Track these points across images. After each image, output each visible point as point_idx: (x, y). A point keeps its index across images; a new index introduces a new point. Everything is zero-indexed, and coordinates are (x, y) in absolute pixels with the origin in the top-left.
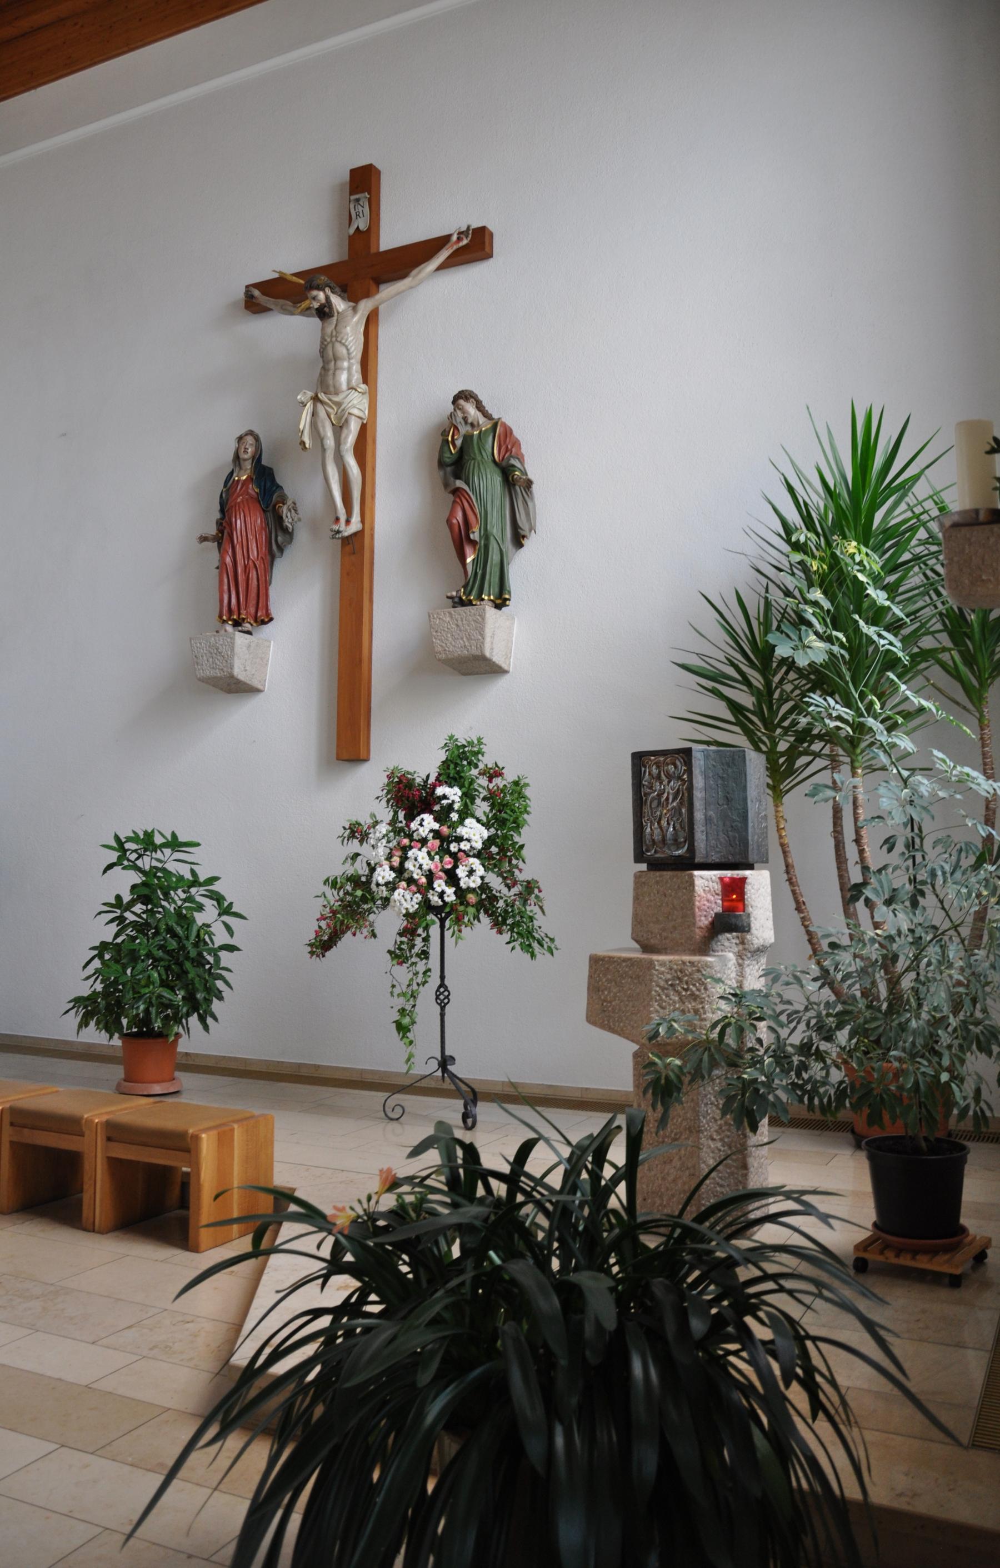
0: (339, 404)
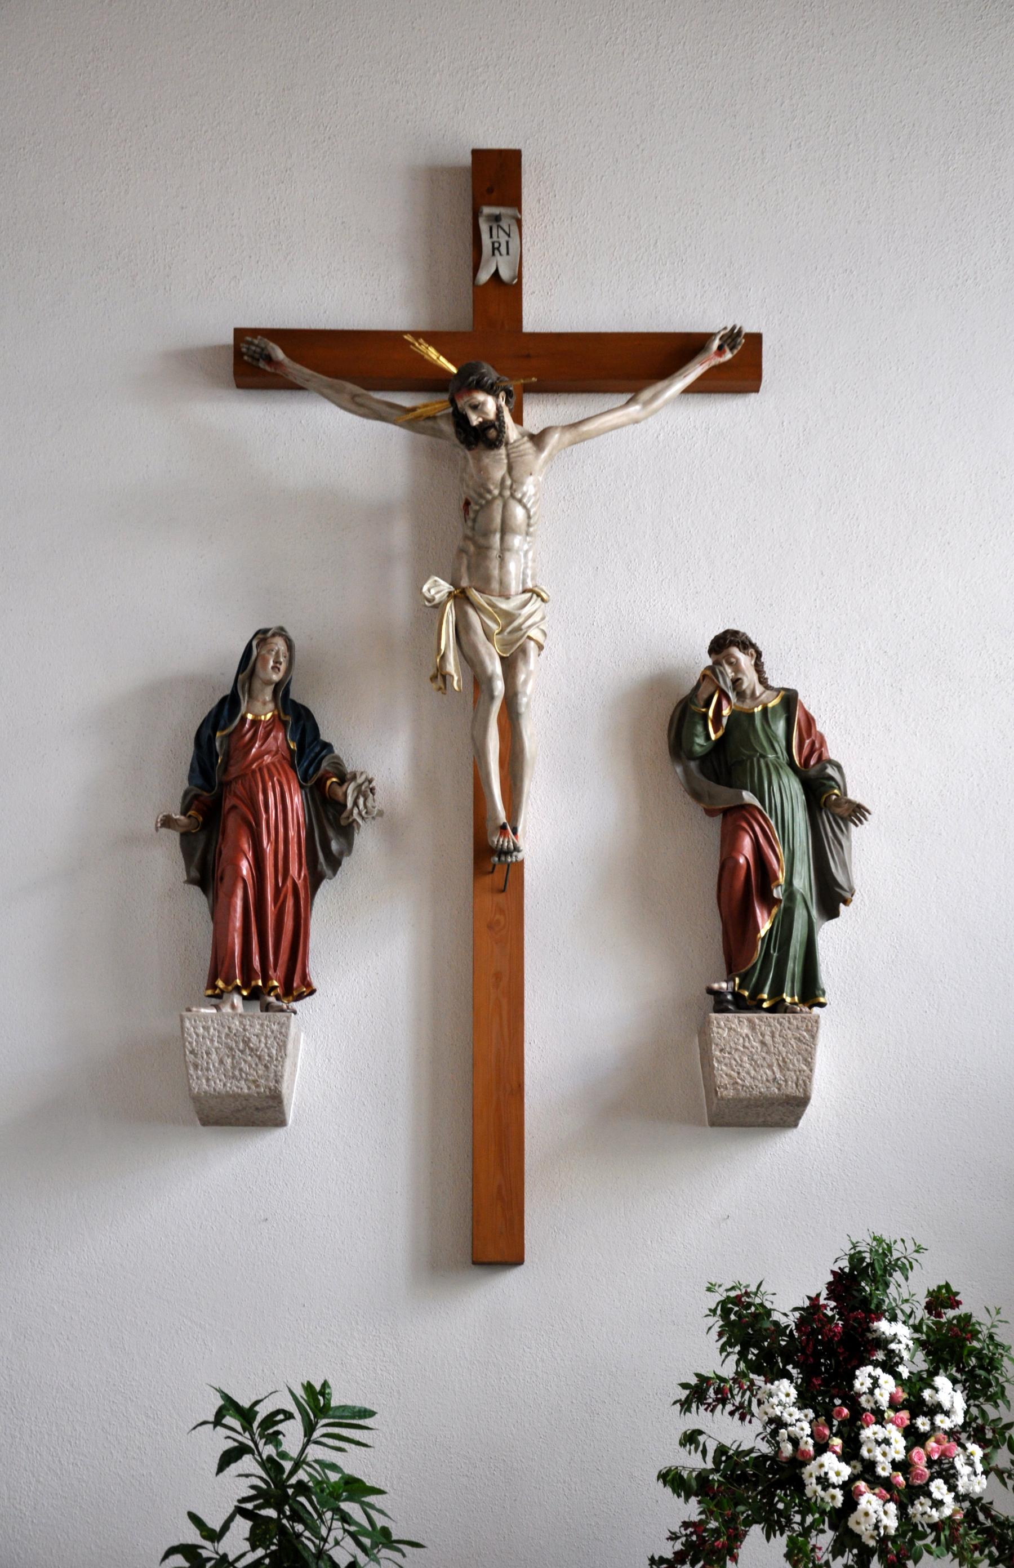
0: (509, 617)
